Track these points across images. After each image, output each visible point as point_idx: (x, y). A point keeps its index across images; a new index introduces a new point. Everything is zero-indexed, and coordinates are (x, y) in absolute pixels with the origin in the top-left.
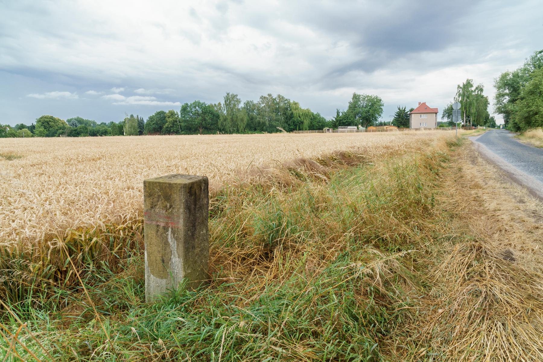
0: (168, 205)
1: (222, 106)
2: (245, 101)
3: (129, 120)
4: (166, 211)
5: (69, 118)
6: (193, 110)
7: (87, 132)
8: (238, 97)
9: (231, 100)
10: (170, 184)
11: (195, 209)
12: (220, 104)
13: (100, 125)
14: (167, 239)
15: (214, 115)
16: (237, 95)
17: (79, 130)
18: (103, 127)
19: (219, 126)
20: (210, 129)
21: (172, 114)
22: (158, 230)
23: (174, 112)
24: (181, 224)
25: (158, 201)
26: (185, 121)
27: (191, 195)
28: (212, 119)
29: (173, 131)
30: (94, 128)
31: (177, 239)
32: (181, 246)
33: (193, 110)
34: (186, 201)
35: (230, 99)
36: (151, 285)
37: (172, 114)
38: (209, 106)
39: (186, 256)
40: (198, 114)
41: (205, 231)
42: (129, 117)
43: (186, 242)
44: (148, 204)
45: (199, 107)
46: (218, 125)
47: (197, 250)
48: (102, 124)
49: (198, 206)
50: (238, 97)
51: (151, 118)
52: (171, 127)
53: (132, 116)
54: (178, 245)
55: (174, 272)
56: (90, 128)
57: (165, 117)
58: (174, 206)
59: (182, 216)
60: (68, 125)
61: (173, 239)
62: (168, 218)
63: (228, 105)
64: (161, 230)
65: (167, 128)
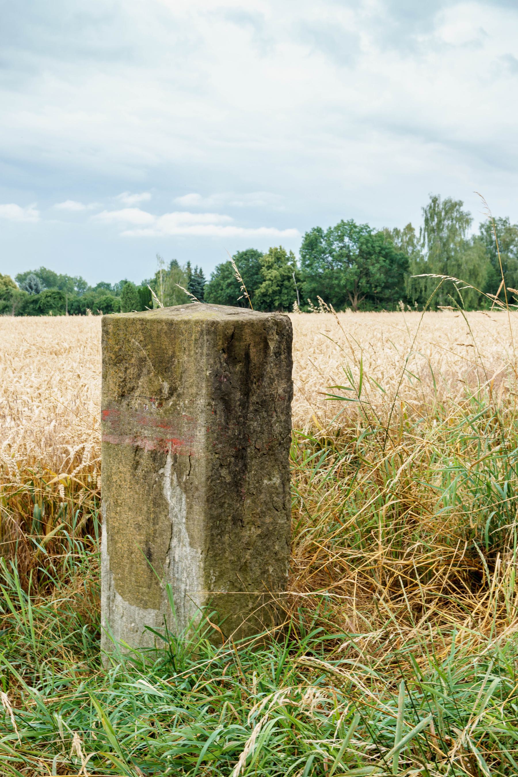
0: (166, 386)
1: (417, 233)
2: (485, 219)
3: (167, 274)
4: (160, 405)
5: (22, 272)
6: (336, 246)
7: (62, 307)
8: (464, 209)
9: (442, 215)
10: (171, 323)
11: (244, 405)
12: (409, 228)
13: (94, 290)
14: (161, 488)
15: (392, 261)
16: (460, 204)
17: (43, 301)
18: (103, 294)
19: (408, 291)
20: (381, 300)
21: (279, 257)
22: (138, 463)
23: (284, 254)
24: (198, 442)
25: (139, 376)
26: (312, 278)
27: (232, 360)
28: (387, 272)
29: (280, 305)
30: (81, 297)
31: (187, 488)
32: (199, 508)
33: (336, 246)
34: (216, 375)
35: (439, 214)
36: (116, 626)
37: (278, 259)
38: (380, 236)
39: (212, 541)
40: (348, 256)
41: (276, 481)
42: (166, 267)
43: (213, 499)
44: (112, 386)
45: (351, 237)
46: (403, 289)
47: (251, 533)
48: (100, 285)
49: (254, 399)
50: (464, 209)
51: (224, 270)
52: (274, 292)
53: (174, 264)
54: (190, 507)
55: (177, 590)
56: (69, 297)
57: (259, 267)
58: (180, 390)
59: (201, 420)
60: (18, 288)
61: (178, 489)
62: (165, 425)
63: (433, 230)
64: (145, 461)
65: (264, 295)
